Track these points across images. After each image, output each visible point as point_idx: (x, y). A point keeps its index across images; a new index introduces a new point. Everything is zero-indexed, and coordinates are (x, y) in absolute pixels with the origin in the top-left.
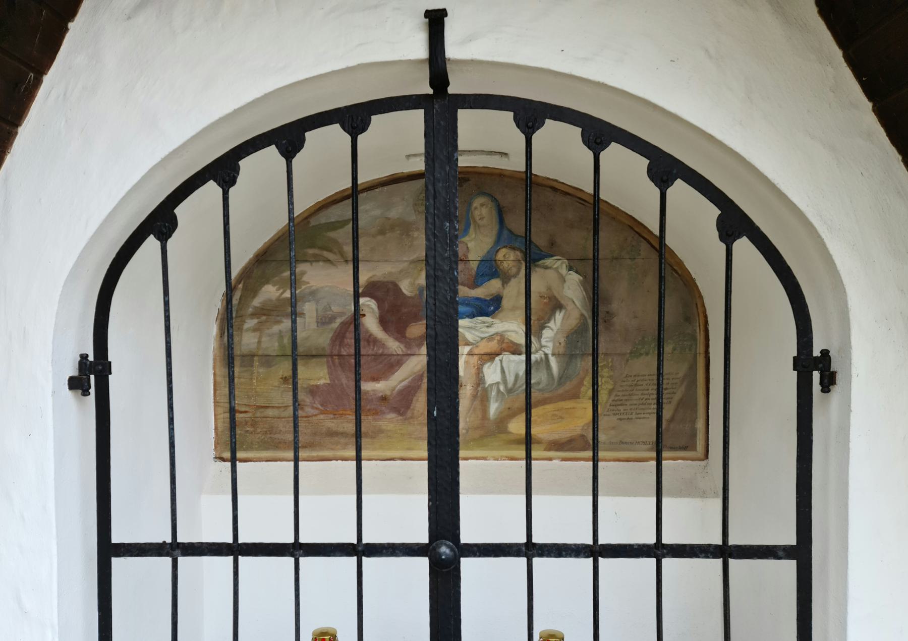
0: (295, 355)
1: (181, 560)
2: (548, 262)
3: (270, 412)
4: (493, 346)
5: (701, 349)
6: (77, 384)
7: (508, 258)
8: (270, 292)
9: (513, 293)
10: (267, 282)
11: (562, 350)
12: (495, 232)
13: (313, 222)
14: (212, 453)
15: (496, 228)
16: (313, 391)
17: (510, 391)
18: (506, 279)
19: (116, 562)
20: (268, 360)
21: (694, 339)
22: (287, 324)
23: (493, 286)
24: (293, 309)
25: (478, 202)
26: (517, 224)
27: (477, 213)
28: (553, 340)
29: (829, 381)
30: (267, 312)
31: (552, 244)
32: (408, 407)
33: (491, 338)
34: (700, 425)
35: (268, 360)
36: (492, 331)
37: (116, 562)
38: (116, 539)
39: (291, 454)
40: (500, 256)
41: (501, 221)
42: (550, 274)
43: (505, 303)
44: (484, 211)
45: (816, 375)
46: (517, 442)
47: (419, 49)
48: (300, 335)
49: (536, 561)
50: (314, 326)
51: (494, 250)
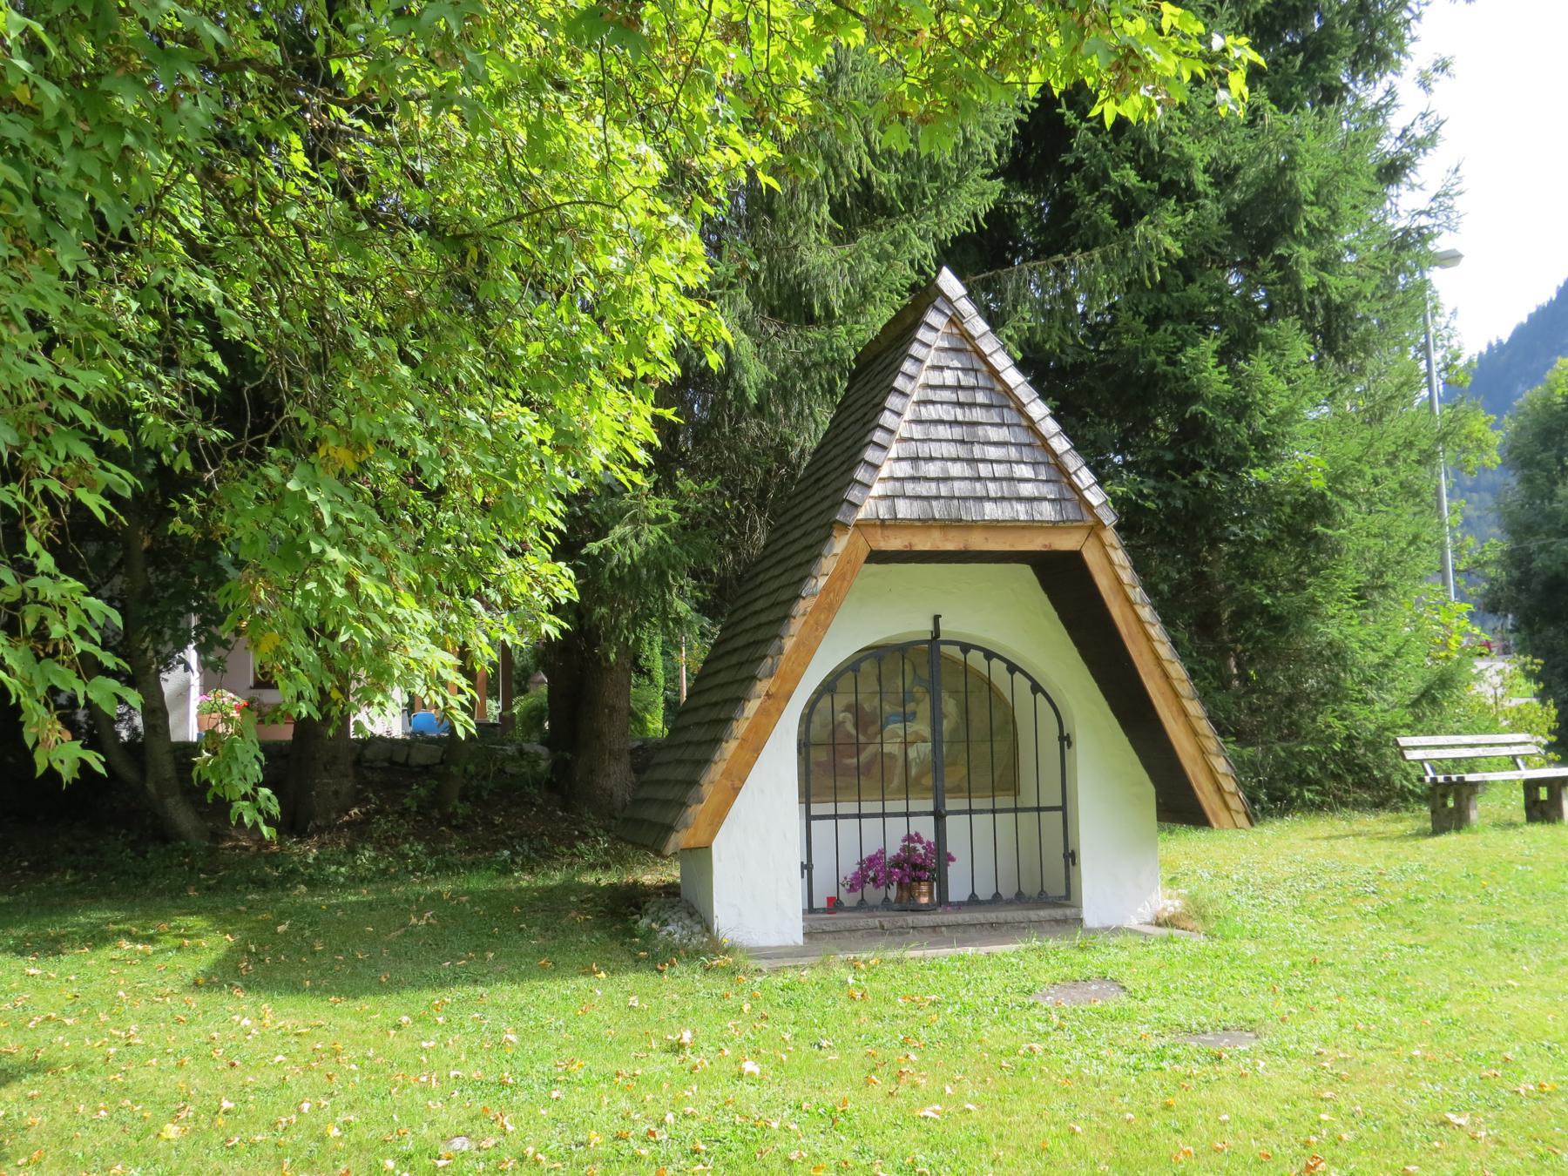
16: (818, 764)
19: (813, 823)
29: (1070, 745)
37: (813, 823)
47: (930, 627)
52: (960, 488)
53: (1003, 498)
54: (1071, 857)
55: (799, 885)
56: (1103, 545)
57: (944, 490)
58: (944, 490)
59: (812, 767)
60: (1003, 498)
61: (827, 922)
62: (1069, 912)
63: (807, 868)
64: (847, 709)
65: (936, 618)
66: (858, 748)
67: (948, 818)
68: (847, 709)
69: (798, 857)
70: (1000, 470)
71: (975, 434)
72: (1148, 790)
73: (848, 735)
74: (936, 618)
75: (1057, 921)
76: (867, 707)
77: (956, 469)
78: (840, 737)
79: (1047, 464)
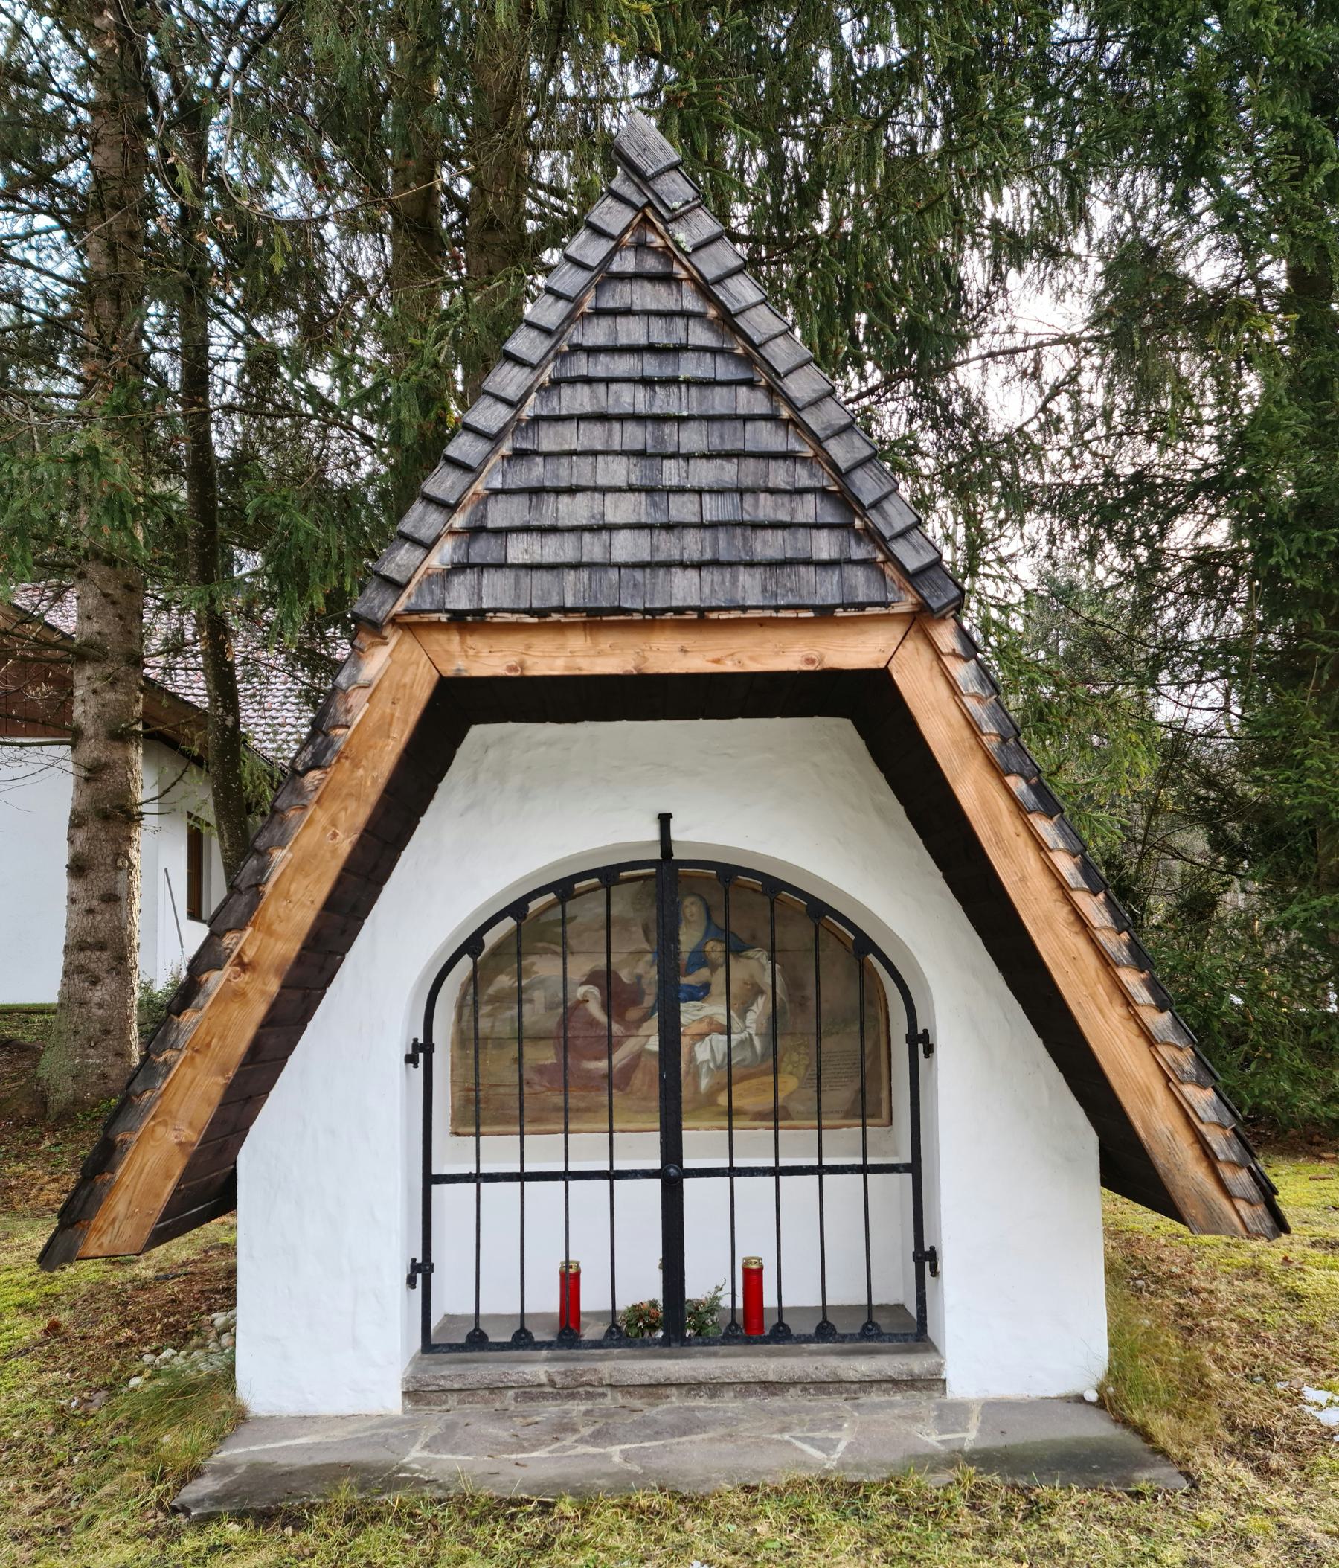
0: (520, 1037)
1: (483, 1185)
2: (750, 953)
3: (502, 1090)
4: (703, 1027)
5: (883, 1028)
6: (411, 1059)
7: (715, 950)
8: (505, 981)
9: (718, 980)
10: (501, 972)
11: (763, 1030)
12: (703, 929)
13: (543, 919)
14: (449, 1129)
15: (704, 923)
16: (541, 1070)
17: (718, 1068)
18: (714, 968)
19: (435, 1188)
20: (500, 1043)
21: (877, 1019)
22: (516, 1011)
23: (703, 974)
24: (520, 996)
25: (688, 901)
26: (719, 920)
27: (687, 912)
28: (756, 1021)
29: (929, 1050)
30: (497, 999)
31: (754, 937)
32: (627, 1083)
33: (701, 1020)
34: (884, 1094)
35: (500, 1043)
36: (702, 1014)
37: (435, 1188)
38: (435, 1171)
39: (517, 1129)
40: (708, 948)
41: (709, 918)
42: (753, 963)
43: (713, 989)
44: (694, 909)
45: (921, 1047)
46: (721, 1114)
47: (653, 834)
48: (526, 1020)
49: (736, 1179)
50: (542, 1011)
51: (703, 943)
52: (626, 547)
53: (716, 563)
54: (926, 1259)
55: (403, 1305)
56: (938, 654)
57: (593, 548)
58: (593, 548)
59: (527, 1075)
60: (716, 563)
61: (447, 1372)
62: (917, 1364)
63: (421, 1271)
64: (592, 979)
65: (665, 820)
66: (611, 1045)
67: (688, 1183)
68: (592, 979)
69: (404, 1248)
70: (714, 509)
71: (659, 440)
72: (1089, 1141)
73: (593, 1023)
74: (665, 820)
75: (896, 1383)
76: (625, 976)
77: (621, 509)
78: (576, 1029)
79: (823, 492)
